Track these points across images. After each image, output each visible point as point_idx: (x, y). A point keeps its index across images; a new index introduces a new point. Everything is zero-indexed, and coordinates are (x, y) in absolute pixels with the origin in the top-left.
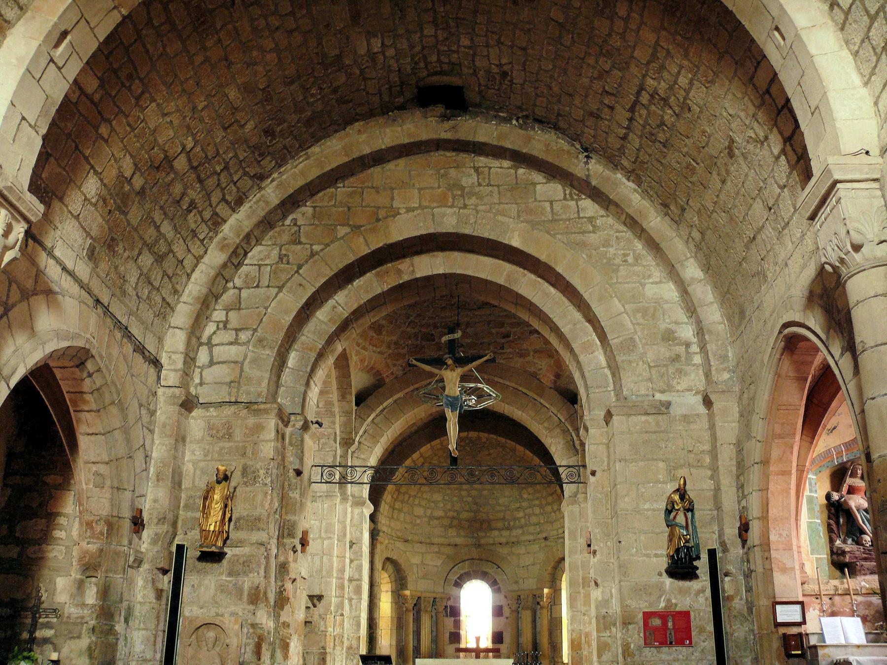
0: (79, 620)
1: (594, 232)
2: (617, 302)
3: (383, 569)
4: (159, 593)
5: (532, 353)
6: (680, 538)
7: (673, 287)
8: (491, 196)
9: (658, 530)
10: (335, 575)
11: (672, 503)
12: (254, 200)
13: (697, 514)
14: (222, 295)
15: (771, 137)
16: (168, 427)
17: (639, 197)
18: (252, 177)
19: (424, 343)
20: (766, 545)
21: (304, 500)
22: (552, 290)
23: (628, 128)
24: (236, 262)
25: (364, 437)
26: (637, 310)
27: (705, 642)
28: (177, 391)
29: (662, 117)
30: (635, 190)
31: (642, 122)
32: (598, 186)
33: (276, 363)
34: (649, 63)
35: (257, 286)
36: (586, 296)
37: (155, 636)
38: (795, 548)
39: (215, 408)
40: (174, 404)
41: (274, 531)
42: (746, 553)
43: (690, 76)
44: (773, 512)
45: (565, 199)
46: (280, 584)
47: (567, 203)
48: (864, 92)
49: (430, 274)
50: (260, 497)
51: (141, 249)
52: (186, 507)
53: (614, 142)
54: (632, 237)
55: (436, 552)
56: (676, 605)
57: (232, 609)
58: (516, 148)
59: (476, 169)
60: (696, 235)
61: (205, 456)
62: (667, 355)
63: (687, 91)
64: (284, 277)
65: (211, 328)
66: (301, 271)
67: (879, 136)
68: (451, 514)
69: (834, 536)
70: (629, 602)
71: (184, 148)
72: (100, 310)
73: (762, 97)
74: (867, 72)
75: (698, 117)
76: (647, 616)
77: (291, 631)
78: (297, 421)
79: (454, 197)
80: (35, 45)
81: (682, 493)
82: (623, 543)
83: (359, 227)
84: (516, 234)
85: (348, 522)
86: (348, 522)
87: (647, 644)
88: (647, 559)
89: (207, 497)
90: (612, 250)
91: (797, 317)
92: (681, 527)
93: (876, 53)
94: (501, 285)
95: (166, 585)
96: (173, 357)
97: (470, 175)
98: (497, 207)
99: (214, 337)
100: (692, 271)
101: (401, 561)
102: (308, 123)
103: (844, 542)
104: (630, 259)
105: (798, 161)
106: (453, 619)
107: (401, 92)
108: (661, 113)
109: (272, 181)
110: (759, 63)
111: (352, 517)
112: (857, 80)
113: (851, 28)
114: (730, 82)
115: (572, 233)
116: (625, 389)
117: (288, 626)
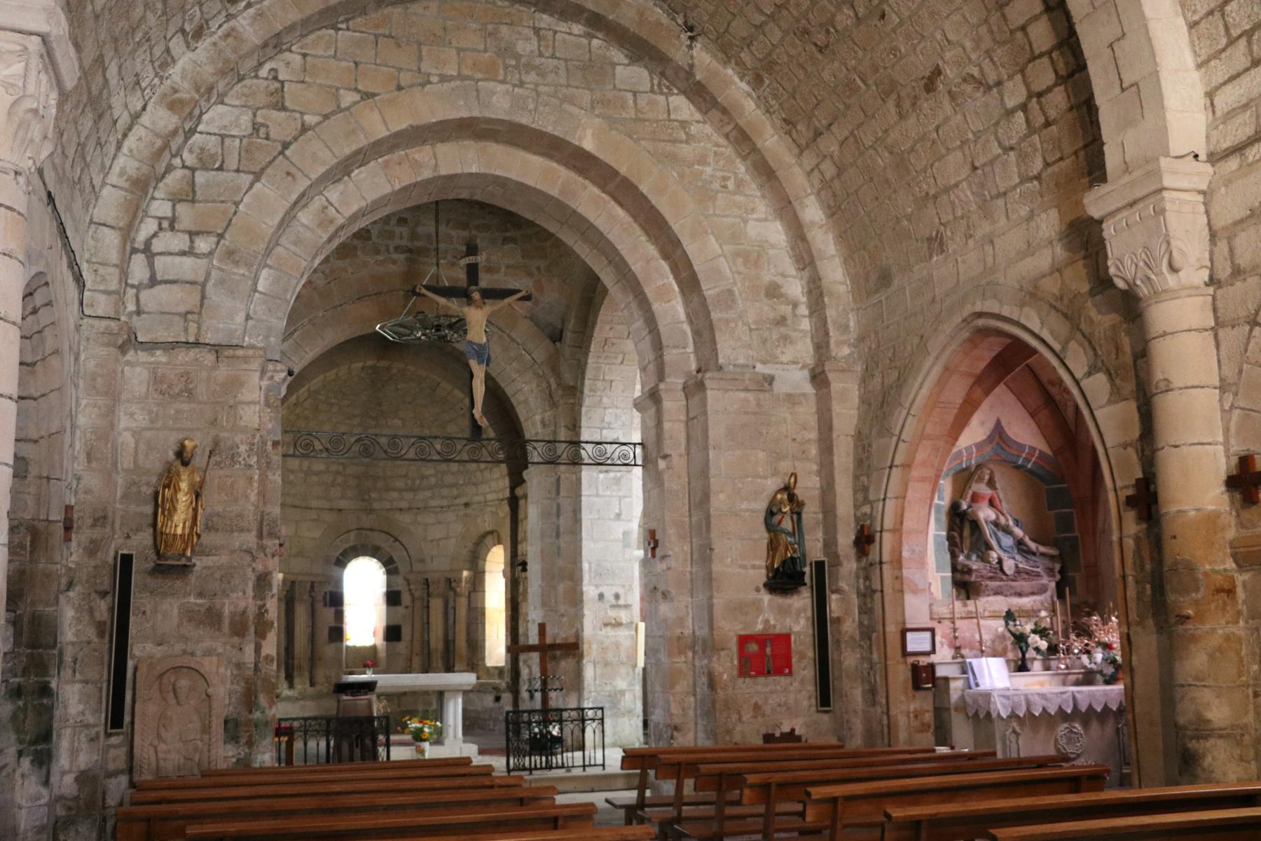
1: (687, 142)
2: (712, 239)
4: (100, 628)
6: (787, 549)
7: (780, 228)
8: (557, 73)
9: (756, 536)
12: (220, 33)
14: (163, 177)
15: (1009, 85)
16: (99, 379)
17: (753, 106)
22: (620, 212)
23: (772, 17)
26: (737, 254)
27: (805, 670)
29: (833, 16)
30: (749, 95)
31: (795, 13)
32: (703, 82)
35: (220, 169)
36: (676, 228)
39: (164, 350)
40: (108, 345)
44: (907, 524)
45: (652, 91)
46: (260, 603)
48: (1195, 76)
52: (125, 496)
53: (740, 29)
54: (734, 155)
55: (313, 520)
56: (774, 627)
57: (207, 644)
59: (537, 31)
60: (828, 169)
61: (152, 422)
62: (772, 315)
64: (262, 159)
66: (287, 152)
67: (1207, 137)
69: (957, 550)
73: (1012, 32)
76: (743, 640)
78: (275, 371)
79: (506, 68)
83: (373, 95)
84: (589, 133)
87: (743, 672)
88: (743, 572)
89: (169, 480)
90: (709, 170)
92: (788, 534)
96: (101, 270)
97: (528, 39)
98: (564, 90)
99: (154, 241)
100: (812, 212)
103: (968, 557)
104: (731, 184)
106: (333, 609)
108: (833, 10)
112: (1189, 59)
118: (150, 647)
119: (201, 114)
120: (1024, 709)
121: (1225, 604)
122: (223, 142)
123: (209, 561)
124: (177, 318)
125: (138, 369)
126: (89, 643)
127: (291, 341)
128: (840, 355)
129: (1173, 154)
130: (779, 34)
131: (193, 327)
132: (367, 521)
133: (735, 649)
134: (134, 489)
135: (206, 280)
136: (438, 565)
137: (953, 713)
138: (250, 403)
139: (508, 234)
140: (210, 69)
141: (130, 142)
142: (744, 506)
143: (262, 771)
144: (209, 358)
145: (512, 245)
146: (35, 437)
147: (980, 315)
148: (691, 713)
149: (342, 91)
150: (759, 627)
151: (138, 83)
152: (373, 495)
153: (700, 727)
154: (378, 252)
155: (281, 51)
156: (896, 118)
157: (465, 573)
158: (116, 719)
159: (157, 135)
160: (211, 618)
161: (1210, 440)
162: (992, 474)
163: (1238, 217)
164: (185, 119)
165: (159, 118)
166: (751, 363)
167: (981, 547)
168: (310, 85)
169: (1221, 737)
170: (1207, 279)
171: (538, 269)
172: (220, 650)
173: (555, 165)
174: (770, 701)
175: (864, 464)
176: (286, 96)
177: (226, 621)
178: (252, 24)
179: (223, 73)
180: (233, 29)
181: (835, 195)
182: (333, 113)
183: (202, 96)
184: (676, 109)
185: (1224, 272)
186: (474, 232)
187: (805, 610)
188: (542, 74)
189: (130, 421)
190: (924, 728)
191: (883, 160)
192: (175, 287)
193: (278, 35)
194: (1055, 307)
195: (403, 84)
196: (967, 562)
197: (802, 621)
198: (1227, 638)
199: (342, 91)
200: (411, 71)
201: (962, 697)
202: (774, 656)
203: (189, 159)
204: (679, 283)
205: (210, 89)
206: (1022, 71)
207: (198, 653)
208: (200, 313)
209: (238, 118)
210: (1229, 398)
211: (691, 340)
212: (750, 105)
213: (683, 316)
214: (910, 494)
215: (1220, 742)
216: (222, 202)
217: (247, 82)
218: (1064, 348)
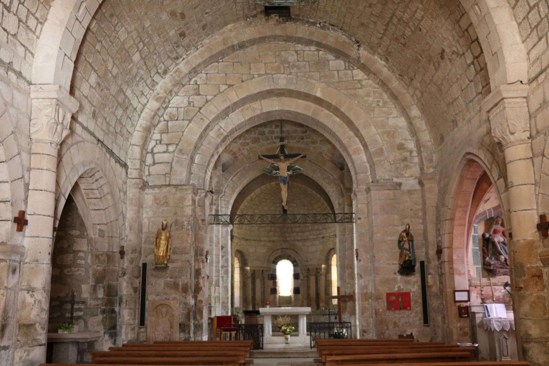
0: (96, 307)
1: (361, 88)
2: (373, 127)
4: (135, 290)
5: (319, 142)
10: (214, 265)
11: (403, 237)
12: (173, 71)
13: (415, 242)
14: (157, 125)
15: (466, 54)
16: (134, 201)
18: (172, 59)
19: (259, 136)
20: (451, 261)
23: (384, 34)
24: (164, 106)
26: (384, 133)
27: (417, 308)
28: (138, 181)
29: (404, 32)
30: (385, 66)
34: (399, 3)
35: (177, 120)
36: (357, 124)
37: (135, 312)
38: (466, 262)
40: (136, 188)
41: (192, 253)
42: (440, 264)
43: (422, 13)
44: (455, 244)
45: (345, 69)
46: (196, 280)
48: (522, 46)
49: (271, 110)
51: (117, 106)
52: (145, 242)
54: (382, 91)
56: (403, 289)
57: (174, 296)
58: (319, 41)
59: (296, 52)
61: (154, 214)
62: (400, 157)
63: (420, 21)
64: (192, 114)
65: (152, 144)
66: (201, 111)
67: (528, 72)
69: (485, 255)
70: (379, 288)
71: (138, 48)
72: (100, 145)
73: (463, 32)
74: (525, 36)
75: (425, 35)
76: (389, 295)
77: (203, 304)
78: (201, 193)
79: (284, 68)
80: (69, 11)
81: (407, 232)
83: (233, 85)
84: (319, 89)
85: (220, 236)
86: (220, 236)
87: (388, 309)
89: (158, 237)
90: (371, 99)
91: (475, 152)
92: (406, 250)
93: (531, 27)
94: (309, 117)
95: (138, 285)
96: (134, 161)
97: (293, 55)
98: (308, 74)
99: (155, 149)
100: (415, 112)
101: (245, 251)
102: (204, 27)
103: (491, 259)
104: (381, 104)
105: (481, 70)
106: (272, 281)
107: (255, 8)
109: (184, 59)
110: (463, 15)
111: (222, 232)
112: (518, 39)
113: (518, 9)
114: (446, 20)
116: (377, 176)
118: (154, 297)
119: (170, 101)
120: (509, 328)
121: (537, 282)
123: (174, 265)
124: (162, 176)
125: (149, 196)
126: (131, 295)
127: (236, 177)
128: (429, 172)
129: (509, 82)
130: (388, 41)
131: (168, 179)
133: (385, 299)
134: (148, 239)
135: (173, 161)
136: (313, 262)
137: (478, 328)
138: (187, 206)
140: (170, 84)
141: (143, 115)
142: (389, 238)
143: (205, 342)
144: (173, 190)
146: (105, 222)
147: (469, 153)
149: (221, 86)
150: (396, 289)
151: (143, 94)
154: (268, 139)
155: (198, 73)
156: (435, 71)
158: (142, 322)
159: (152, 111)
160: (175, 286)
161: (530, 208)
162: (502, 221)
163: (537, 108)
164: (162, 104)
165: (153, 105)
166: (391, 178)
167: (497, 254)
169: (536, 342)
170: (529, 136)
172: (178, 298)
173: (309, 103)
174: (401, 321)
175: (439, 221)
176: (200, 90)
177: (180, 287)
178: (184, 66)
179: (175, 85)
180: (178, 69)
181: (423, 105)
182: (218, 94)
183: (167, 95)
185: (534, 133)
187: (417, 282)
189: (147, 215)
190: (465, 334)
191: (434, 89)
192: (162, 165)
193: (194, 68)
194: (488, 149)
196: (490, 261)
197: (416, 287)
198: (538, 297)
199: (221, 86)
201: (482, 321)
202: (403, 302)
203: (166, 117)
204: (363, 146)
205: (171, 92)
206: (470, 48)
207: (171, 299)
208: (170, 174)
210: (537, 188)
212: (385, 70)
213: (365, 160)
214: (455, 232)
215: (535, 345)
217: (186, 87)
218: (491, 168)
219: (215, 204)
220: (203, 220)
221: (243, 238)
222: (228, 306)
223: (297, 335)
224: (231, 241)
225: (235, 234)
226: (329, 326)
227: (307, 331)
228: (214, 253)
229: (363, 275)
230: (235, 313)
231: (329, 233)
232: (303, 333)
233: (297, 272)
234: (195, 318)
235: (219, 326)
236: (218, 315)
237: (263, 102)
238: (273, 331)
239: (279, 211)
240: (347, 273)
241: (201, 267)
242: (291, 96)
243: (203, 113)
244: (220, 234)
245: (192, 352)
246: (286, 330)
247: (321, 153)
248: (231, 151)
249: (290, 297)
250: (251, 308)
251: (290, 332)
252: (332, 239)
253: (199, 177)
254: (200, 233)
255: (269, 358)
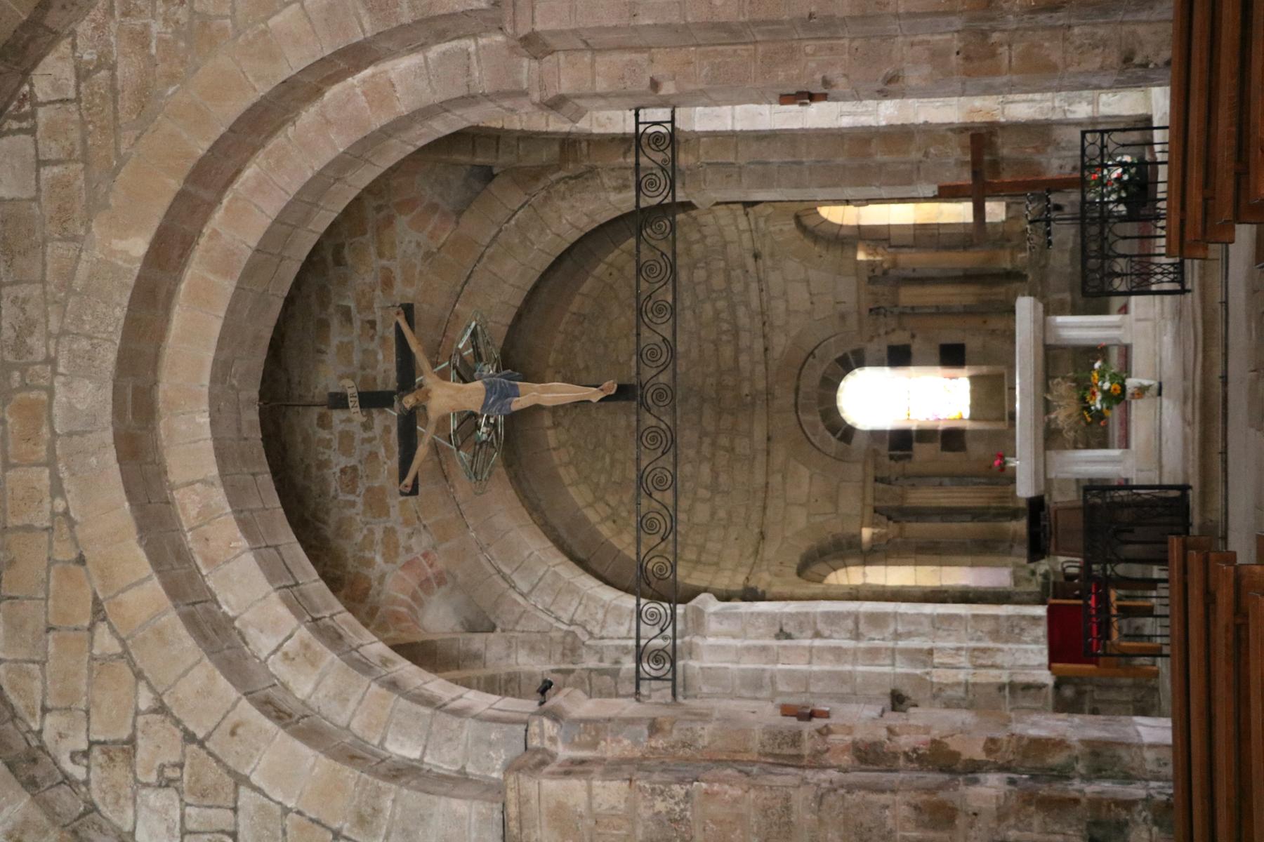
1: (113, 68)
3: (820, 582)
5: (384, 262)
8: (25, 301)
10: (848, 668)
19: (361, 489)
21: (716, 715)
22: (249, 172)
25: (560, 613)
33: (414, 783)
36: (263, 89)
41: (786, 778)
45: (32, 131)
46: (901, 762)
47: (41, 128)
49: (210, 444)
50: (713, 808)
64: (212, 774)
66: (200, 735)
68: (706, 450)
77: (1001, 735)
78: (542, 735)
79: (25, 387)
82: (813, 9)
84: (118, 245)
85: (738, 643)
86: (738, 643)
90: (156, 27)
98: (51, 288)
101: (803, 546)
106: (915, 445)
111: (726, 635)
115: (116, 118)
117: (993, 741)
122: (191, 833)
127: (515, 577)
132: (784, 398)
136: (848, 292)
139: (330, 258)
145: (346, 251)
148: (1101, 32)
149: (96, 652)
152: (746, 391)
153: (1128, 18)
154: (373, 456)
155: (42, 747)
157: (861, 256)
168: (91, 702)
171: (379, 209)
173: (183, 286)
176: (111, 737)
184: (57, 87)
186: (331, 310)
188: (28, 327)
195: (74, 555)
199: (96, 652)
200: (50, 542)
204: (358, 69)
209: (153, 810)
211: (454, 43)
213: (414, 60)
216: (284, 833)
217: (96, 797)
219: (617, 662)
220: (655, 728)
221: (756, 552)
222: (1009, 617)
223: (1126, 350)
224: (762, 598)
225: (737, 582)
226: (1092, 220)
227: (1104, 311)
228: (803, 667)
229: (888, 70)
230: (1034, 587)
231: (740, 232)
232: (1118, 327)
233: (884, 353)
234: (1063, 774)
235: (1088, 657)
236: (1044, 658)
237: (176, 474)
238: (1104, 445)
239: (623, 419)
240: (886, 158)
241: (848, 739)
242: (154, 362)
243: (211, 725)
244: (731, 642)
245: (1196, 782)
246: (1107, 395)
247: (428, 255)
248: (414, 597)
249: (974, 379)
250: (1020, 526)
251: (1113, 378)
252: (762, 224)
253: (478, 740)
254: (704, 741)
255: (1225, 462)
